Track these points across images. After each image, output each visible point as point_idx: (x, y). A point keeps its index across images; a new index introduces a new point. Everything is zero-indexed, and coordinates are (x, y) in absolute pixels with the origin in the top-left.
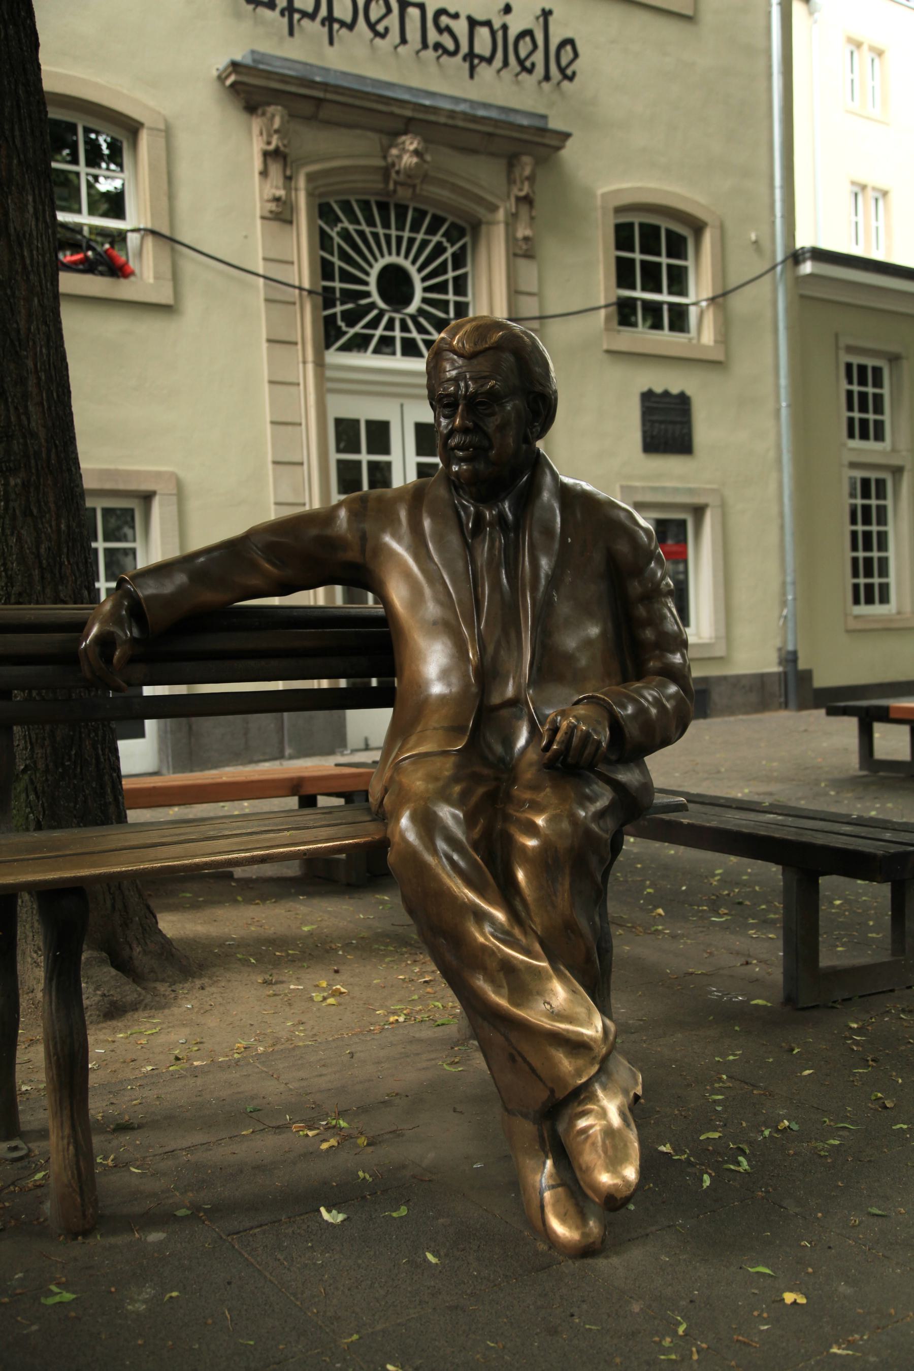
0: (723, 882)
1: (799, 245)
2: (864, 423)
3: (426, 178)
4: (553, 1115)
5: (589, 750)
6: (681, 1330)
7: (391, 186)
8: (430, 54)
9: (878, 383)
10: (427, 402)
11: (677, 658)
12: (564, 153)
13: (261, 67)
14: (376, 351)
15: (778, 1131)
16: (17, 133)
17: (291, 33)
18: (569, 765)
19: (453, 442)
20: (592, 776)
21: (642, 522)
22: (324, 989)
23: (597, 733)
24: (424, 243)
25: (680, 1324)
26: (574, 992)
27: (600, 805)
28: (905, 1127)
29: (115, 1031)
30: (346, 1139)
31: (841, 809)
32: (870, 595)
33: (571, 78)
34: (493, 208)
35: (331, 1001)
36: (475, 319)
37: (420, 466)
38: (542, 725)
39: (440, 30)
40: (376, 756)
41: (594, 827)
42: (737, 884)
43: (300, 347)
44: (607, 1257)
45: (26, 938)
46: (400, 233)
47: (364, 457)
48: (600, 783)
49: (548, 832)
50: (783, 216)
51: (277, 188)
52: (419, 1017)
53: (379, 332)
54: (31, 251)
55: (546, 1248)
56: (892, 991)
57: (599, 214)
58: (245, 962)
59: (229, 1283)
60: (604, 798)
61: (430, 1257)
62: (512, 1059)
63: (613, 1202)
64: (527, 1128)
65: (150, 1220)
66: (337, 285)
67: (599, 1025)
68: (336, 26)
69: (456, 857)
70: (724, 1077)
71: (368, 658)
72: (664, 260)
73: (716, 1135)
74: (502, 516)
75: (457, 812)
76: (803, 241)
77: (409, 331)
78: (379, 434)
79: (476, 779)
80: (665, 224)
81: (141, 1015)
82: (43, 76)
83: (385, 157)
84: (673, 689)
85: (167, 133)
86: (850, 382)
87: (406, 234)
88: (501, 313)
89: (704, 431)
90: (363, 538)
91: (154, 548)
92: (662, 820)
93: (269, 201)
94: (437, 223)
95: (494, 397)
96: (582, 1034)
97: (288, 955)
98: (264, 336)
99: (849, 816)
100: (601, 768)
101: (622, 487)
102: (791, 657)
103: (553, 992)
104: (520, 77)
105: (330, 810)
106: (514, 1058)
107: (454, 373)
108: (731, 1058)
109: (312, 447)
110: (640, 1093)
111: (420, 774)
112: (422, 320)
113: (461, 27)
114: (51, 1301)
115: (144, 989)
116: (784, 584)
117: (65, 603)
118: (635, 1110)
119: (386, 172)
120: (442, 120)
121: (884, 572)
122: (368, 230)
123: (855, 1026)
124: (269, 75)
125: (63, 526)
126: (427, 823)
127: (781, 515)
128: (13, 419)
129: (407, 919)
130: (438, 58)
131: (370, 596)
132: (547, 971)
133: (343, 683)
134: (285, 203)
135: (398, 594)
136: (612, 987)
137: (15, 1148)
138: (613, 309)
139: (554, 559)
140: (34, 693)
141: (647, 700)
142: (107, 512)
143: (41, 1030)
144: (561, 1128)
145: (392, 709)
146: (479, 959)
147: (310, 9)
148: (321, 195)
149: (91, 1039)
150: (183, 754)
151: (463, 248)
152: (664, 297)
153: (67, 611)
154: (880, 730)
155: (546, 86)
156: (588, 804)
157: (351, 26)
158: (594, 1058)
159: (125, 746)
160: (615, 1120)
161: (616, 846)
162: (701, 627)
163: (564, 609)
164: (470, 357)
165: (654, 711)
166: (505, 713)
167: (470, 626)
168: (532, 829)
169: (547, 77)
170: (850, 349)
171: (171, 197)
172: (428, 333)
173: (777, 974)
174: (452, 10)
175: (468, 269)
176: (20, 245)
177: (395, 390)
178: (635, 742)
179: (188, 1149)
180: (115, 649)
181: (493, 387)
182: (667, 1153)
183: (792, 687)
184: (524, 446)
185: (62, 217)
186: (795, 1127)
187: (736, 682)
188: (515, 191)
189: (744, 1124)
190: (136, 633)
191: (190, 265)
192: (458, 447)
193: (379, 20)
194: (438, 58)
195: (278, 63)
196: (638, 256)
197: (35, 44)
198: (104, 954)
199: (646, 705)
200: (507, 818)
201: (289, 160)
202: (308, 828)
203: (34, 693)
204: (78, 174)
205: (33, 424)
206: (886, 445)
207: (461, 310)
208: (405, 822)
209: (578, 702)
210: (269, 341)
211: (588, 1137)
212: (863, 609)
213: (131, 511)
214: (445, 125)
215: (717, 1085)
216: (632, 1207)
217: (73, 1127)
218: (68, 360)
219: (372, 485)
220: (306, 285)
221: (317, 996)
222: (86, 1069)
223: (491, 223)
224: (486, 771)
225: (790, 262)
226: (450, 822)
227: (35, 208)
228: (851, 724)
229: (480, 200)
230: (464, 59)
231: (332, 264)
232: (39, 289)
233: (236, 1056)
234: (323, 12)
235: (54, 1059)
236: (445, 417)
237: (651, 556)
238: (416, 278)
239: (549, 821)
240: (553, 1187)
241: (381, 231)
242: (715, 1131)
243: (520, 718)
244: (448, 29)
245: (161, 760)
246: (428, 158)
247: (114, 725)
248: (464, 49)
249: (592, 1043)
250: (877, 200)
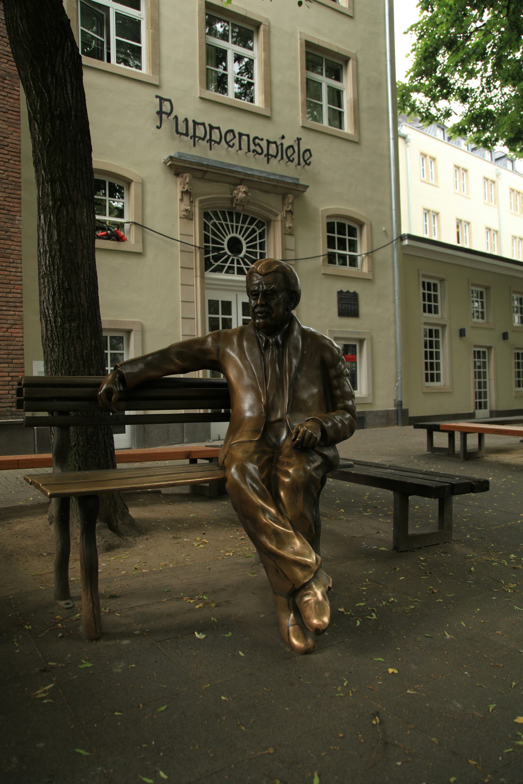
0: (370, 498)
1: (403, 233)
2: (430, 306)
3: (248, 202)
4: (293, 595)
5: (312, 441)
6: (345, 684)
7: (234, 205)
8: (251, 154)
9: (435, 290)
10: (246, 293)
11: (350, 403)
12: (306, 194)
13: (182, 158)
14: (227, 272)
15: (389, 602)
16: (81, 184)
17: (194, 145)
18: (303, 447)
19: (257, 310)
20: (313, 452)
21: (336, 345)
22: (198, 541)
23: (315, 434)
24: (247, 229)
25: (345, 681)
26: (304, 543)
27: (316, 464)
28: (441, 600)
29: (110, 556)
30: (206, 604)
31: (419, 468)
32: (432, 378)
33: (309, 165)
34: (276, 215)
35: (201, 546)
36: (267, 259)
37: (243, 320)
38: (293, 430)
39: (255, 145)
40: (222, 443)
41: (314, 474)
42: (375, 499)
43: (194, 270)
44: (315, 654)
45: (74, 516)
46: (237, 224)
47: (220, 316)
48: (317, 455)
49: (294, 475)
50: (396, 221)
51: (187, 206)
52: (238, 554)
53: (228, 264)
54: (84, 231)
55: (290, 650)
56: (438, 544)
57: (320, 218)
58: (165, 529)
59: (156, 662)
60: (318, 461)
61: (241, 653)
62: (277, 571)
63: (318, 632)
64: (283, 600)
65: (123, 635)
66: (211, 245)
67: (314, 558)
68: (213, 143)
69: (254, 485)
70: (367, 580)
71: (219, 400)
72: (347, 237)
73: (363, 604)
74: (277, 342)
75: (256, 466)
76: (404, 231)
77: (240, 264)
78: (227, 307)
79: (264, 452)
80: (347, 223)
81: (121, 550)
82: (93, 162)
83: (232, 194)
84: (348, 416)
85: (143, 184)
86: (424, 289)
87: (240, 225)
88: (279, 257)
89: (363, 308)
90: (218, 350)
91: (131, 352)
92: (344, 471)
93: (183, 211)
94: (253, 220)
95: (274, 292)
96: (307, 561)
97: (184, 526)
98: (180, 266)
99: (421, 470)
100: (317, 449)
101: (329, 330)
102: (399, 403)
103: (296, 544)
104: (288, 164)
105: (202, 465)
106: (278, 571)
107: (257, 282)
108: (370, 572)
109: (199, 312)
110: (331, 586)
111: (240, 450)
112: (246, 260)
113: (264, 144)
114: (82, 666)
115: (123, 539)
116: (397, 372)
117: (93, 375)
118: (329, 593)
119: (232, 200)
120: (256, 180)
121: (438, 368)
122: (224, 223)
123: (422, 559)
124: (185, 161)
125: (93, 344)
126: (243, 471)
127: (396, 343)
128: (74, 299)
129: (234, 512)
130: (255, 155)
131: (222, 375)
132: (292, 535)
133: (209, 411)
134: (190, 212)
135: (232, 374)
136: (321, 542)
137: (68, 604)
138: (326, 257)
139: (298, 360)
140: (79, 413)
141: (337, 420)
142: (112, 338)
143: (79, 555)
144: (297, 600)
145: (228, 423)
146: (263, 529)
147: (202, 136)
148: (205, 209)
149: (100, 560)
150: (141, 440)
151: (264, 230)
152: (347, 252)
153: (93, 379)
154: (436, 434)
155: (298, 167)
156: (311, 464)
157: (219, 143)
158: (312, 571)
159: (117, 437)
160: (320, 597)
161: (323, 482)
162: (362, 390)
163: (302, 381)
164: (264, 275)
165: (340, 425)
166: (277, 424)
167: (263, 388)
168: (287, 474)
169: (299, 164)
170: (424, 276)
171: (143, 209)
172: (249, 265)
173: (391, 537)
174: (260, 137)
175: (265, 239)
176: (80, 228)
177: (233, 288)
178: (331, 438)
179: (140, 606)
180: (113, 395)
181: (274, 288)
182: (342, 612)
183: (401, 416)
184: (287, 313)
185: (98, 217)
186: (396, 601)
187: (376, 414)
188: (286, 208)
189: (375, 600)
190: (122, 388)
191: (150, 237)
192: (258, 312)
193: (230, 141)
194: (255, 155)
195: (188, 157)
196: (336, 236)
197: (90, 150)
198: (106, 524)
199: (336, 422)
200: (277, 469)
201: (192, 195)
202: (192, 472)
203: (79, 413)
204: (105, 200)
205: (82, 301)
206: (439, 315)
207: (262, 256)
208: (233, 470)
209: (308, 421)
210: (181, 267)
211: (308, 604)
212: (430, 384)
213: (122, 337)
214: (257, 182)
215: (364, 583)
216: (326, 634)
217: (92, 596)
218: (98, 275)
219: (223, 328)
220: (198, 245)
221: (196, 544)
222: (97, 572)
223: (275, 221)
224: (268, 449)
225: (399, 239)
226: (252, 471)
227: (87, 214)
228: (424, 432)
229: (271, 212)
230: (265, 156)
231: (209, 236)
232: (87, 246)
233: (161, 568)
234: (208, 137)
235: (84, 567)
236: (254, 300)
237: (339, 359)
238: (244, 243)
239: (294, 471)
240: (293, 625)
241: (229, 223)
242: (363, 602)
243: (283, 427)
244: (259, 145)
245: (132, 443)
246: (250, 194)
247: (112, 427)
248: (265, 152)
249: (311, 565)
250: (434, 216)
